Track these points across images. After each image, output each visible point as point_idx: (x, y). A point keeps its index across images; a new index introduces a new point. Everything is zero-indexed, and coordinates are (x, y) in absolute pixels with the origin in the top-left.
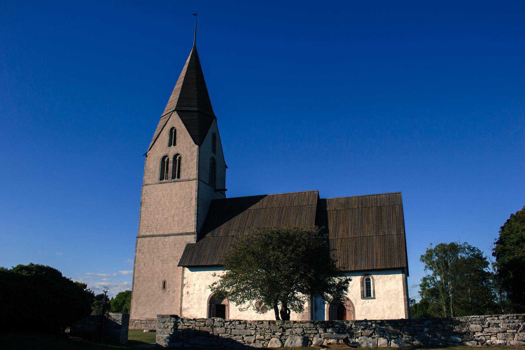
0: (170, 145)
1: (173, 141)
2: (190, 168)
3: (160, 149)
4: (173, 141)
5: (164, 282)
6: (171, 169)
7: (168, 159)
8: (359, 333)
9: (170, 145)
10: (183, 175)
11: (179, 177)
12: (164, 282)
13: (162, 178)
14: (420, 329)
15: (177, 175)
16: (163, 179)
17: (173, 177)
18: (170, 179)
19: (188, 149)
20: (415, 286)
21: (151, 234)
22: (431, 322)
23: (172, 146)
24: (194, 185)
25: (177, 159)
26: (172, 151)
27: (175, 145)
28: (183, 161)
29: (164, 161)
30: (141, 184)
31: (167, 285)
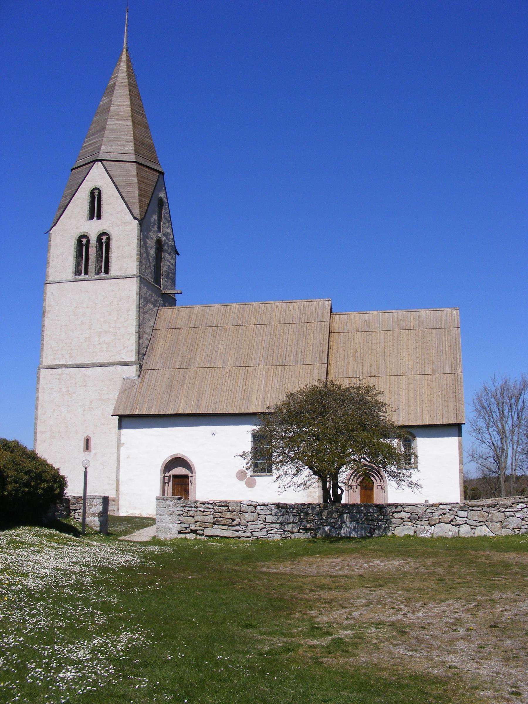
0: (91, 217)
1: (95, 210)
2: (126, 256)
3: (75, 221)
4: (95, 210)
5: (87, 440)
6: (92, 257)
7: (88, 241)
8: (436, 519)
9: (91, 217)
10: (114, 269)
11: (107, 271)
12: (87, 440)
13: (77, 272)
14: (512, 514)
15: (104, 267)
16: (80, 274)
17: (98, 273)
18: (92, 275)
19: (121, 225)
20: (151, 248)
21: (63, 362)
22: (524, 506)
23: (95, 219)
24: (133, 285)
25: (104, 242)
26: (93, 229)
27: (99, 217)
28: (113, 245)
29: (82, 244)
30: (37, 280)
31: (82, 445)
